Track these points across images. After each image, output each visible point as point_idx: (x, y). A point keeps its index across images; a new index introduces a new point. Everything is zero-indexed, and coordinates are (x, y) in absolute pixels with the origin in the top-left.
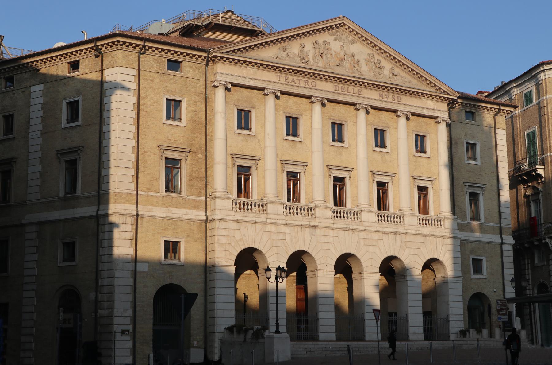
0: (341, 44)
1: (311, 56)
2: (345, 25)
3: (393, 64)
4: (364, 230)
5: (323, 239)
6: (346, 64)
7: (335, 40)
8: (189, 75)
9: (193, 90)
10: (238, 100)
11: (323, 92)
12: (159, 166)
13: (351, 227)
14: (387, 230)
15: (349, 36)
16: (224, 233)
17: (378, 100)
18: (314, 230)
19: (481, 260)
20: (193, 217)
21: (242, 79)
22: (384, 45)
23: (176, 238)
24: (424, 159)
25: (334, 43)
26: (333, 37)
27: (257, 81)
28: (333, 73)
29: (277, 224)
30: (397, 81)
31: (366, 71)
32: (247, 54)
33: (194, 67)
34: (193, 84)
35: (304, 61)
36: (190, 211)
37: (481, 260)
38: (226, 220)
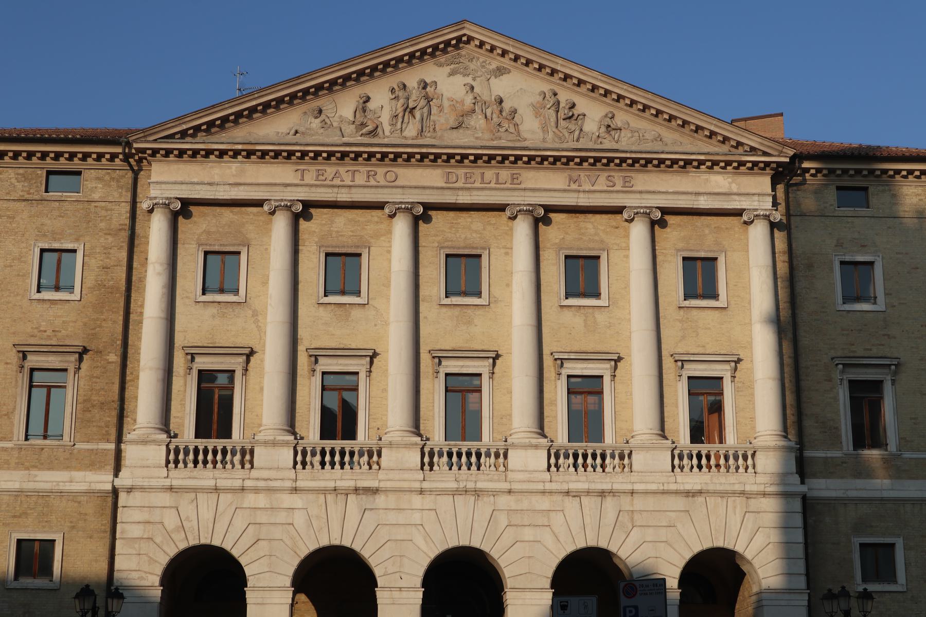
0: (469, 80)
1: (385, 118)
2: (470, 39)
3: (609, 105)
4: (510, 492)
5: (392, 517)
6: (477, 121)
7: (452, 73)
8: (96, 196)
9: (103, 225)
10: (208, 233)
11: (417, 191)
12: (16, 386)
13: (470, 485)
14: (573, 486)
15: (488, 61)
16: (137, 516)
17: (565, 191)
18: (371, 498)
19: (892, 546)
20: (83, 487)
21: (209, 187)
22: (575, 67)
23: (45, 532)
24: (709, 312)
25: (448, 82)
26: (447, 69)
27: (246, 188)
28: (433, 146)
29: (269, 490)
30: (626, 143)
31: (533, 131)
32: (224, 136)
33: (107, 178)
34: (103, 213)
35: (365, 131)
36: (78, 475)
37: (892, 546)
38: (142, 489)
